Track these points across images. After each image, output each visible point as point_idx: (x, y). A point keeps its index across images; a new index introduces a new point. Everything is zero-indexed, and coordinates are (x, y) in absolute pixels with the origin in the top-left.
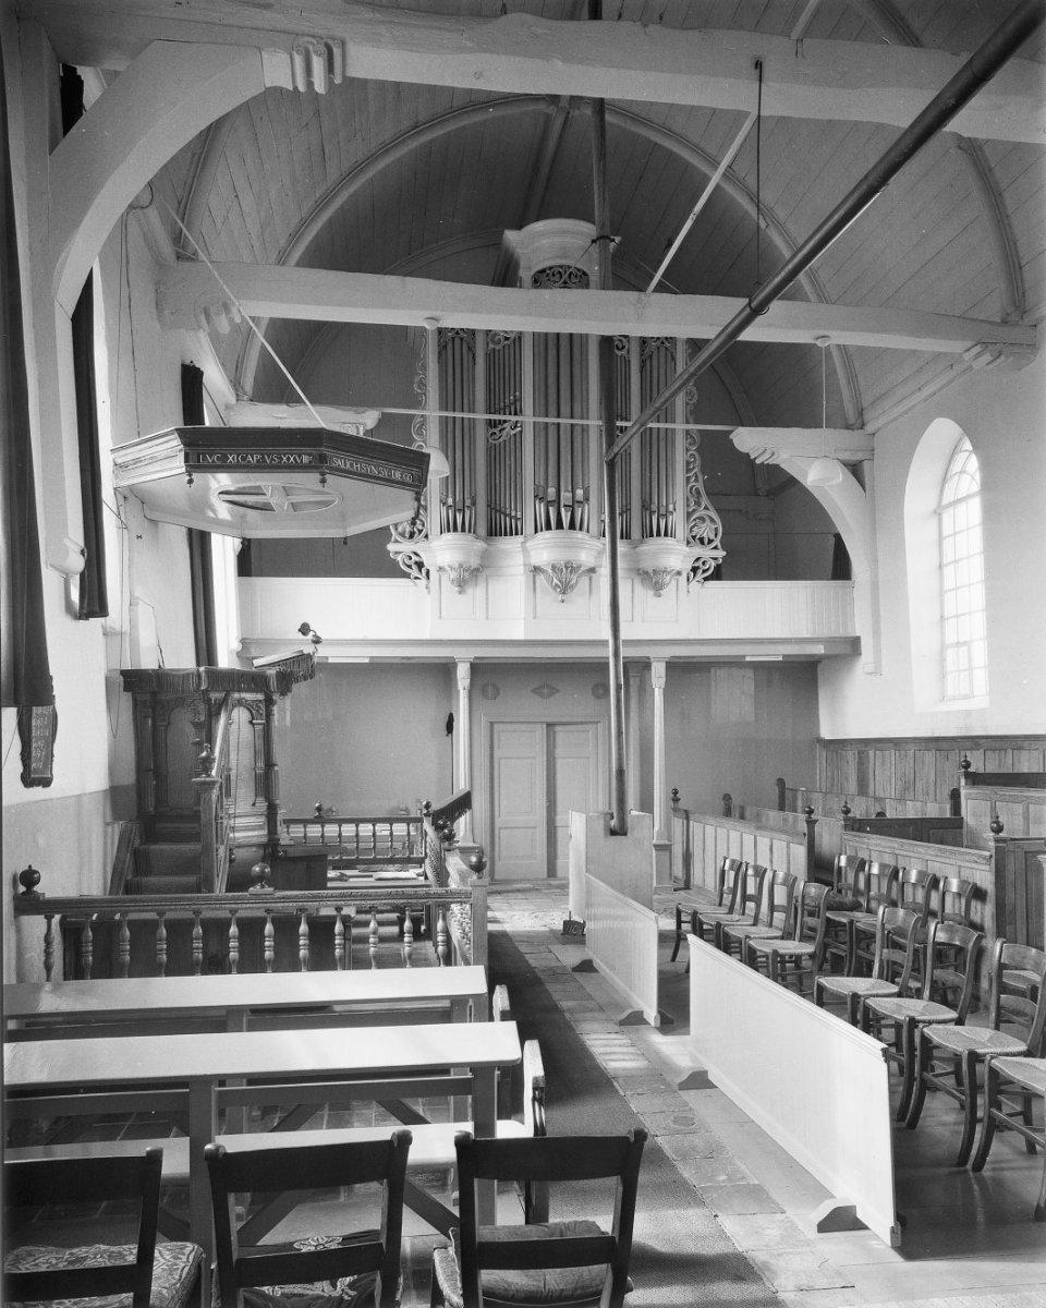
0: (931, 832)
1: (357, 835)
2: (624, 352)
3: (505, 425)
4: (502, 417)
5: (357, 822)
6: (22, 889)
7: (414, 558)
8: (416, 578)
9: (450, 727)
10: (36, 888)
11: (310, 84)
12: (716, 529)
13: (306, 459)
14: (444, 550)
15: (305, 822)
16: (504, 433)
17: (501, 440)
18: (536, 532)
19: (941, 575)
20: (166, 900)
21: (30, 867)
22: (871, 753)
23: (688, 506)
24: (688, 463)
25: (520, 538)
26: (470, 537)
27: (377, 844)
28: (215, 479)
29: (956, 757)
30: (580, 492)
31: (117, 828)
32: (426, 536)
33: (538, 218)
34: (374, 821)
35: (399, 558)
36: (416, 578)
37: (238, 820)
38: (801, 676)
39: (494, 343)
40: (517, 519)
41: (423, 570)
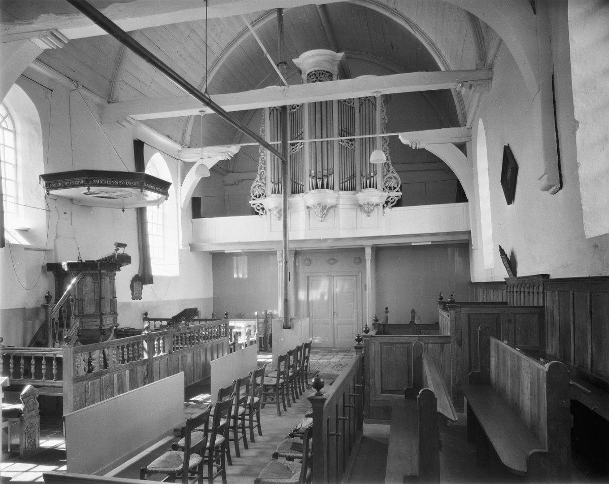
7: (261, 206)
8: (262, 215)
18: (310, 190)
32: (265, 196)
35: (255, 207)
36: (262, 215)
39: (293, 108)
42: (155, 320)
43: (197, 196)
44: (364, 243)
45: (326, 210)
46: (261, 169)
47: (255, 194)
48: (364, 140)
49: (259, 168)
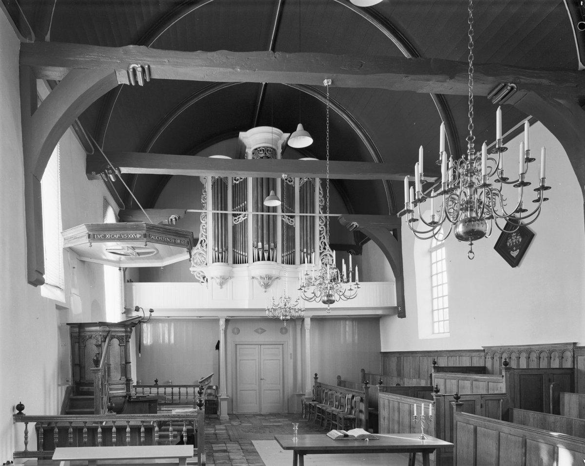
0: (419, 392)
1: (172, 393)
2: (292, 183)
3: (240, 216)
4: (239, 213)
5: (172, 387)
6: (17, 412)
7: (201, 274)
8: (202, 282)
9: (218, 347)
10: (22, 411)
11: (136, 82)
12: (333, 260)
13: (138, 236)
14: (216, 270)
15: (150, 387)
16: (240, 219)
17: (239, 222)
18: (254, 262)
19: (432, 279)
20: (72, 417)
21: (20, 403)
22: (402, 358)
23: (320, 249)
24: (320, 231)
25: (246, 265)
26: (226, 264)
27: (181, 397)
28: (105, 245)
29: (430, 360)
30: (272, 245)
31: (64, 388)
32: (206, 264)
33: (257, 126)
34: (180, 387)
35: (195, 274)
36: (202, 282)
37: (112, 386)
38: (370, 323)
39: (235, 180)
40: (245, 256)
41: (205, 279)
42: (180, 387)
43: (359, 256)
44: (219, 314)
45: (268, 282)
46: (202, 237)
47: (195, 261)
48: (305, 218)
49: (200, 235)
